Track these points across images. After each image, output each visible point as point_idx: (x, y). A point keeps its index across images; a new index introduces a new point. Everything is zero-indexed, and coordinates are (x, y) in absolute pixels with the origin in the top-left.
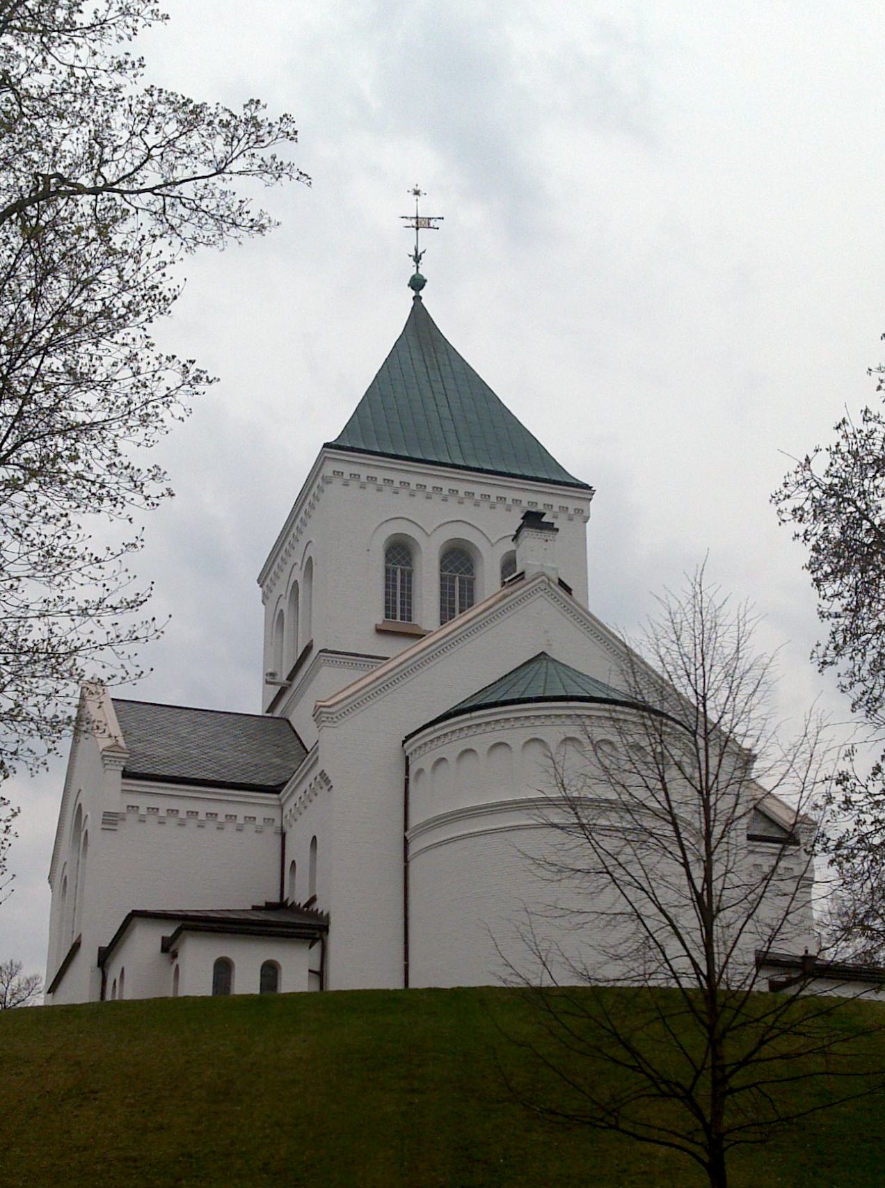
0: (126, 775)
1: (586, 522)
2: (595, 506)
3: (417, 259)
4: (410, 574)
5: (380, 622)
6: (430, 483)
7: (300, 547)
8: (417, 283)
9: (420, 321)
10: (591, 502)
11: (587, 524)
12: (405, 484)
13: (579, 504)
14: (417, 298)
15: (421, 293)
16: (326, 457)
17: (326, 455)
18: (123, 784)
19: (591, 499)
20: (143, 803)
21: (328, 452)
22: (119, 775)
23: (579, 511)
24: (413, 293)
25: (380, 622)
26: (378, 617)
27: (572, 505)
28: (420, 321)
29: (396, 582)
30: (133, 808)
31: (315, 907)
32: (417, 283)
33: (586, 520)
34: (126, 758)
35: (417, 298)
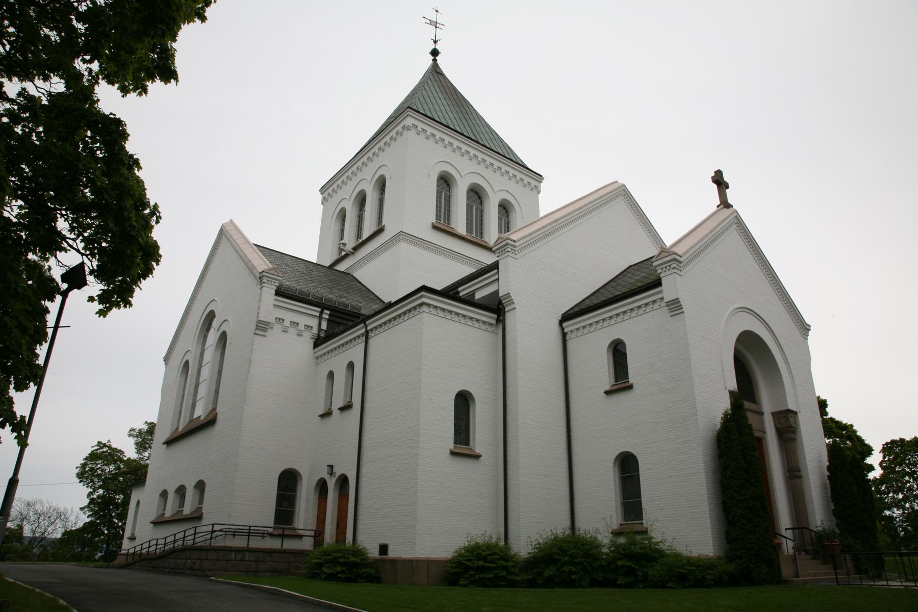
0: (279, 293)
1: (539, 194)
2: (543, 186)
3: (435, 42)
4: (450, 196)
5: (452, 447)
6: (430, 130)
7: (377, 162)
8: (435, 53)
9: (435, 71)
10: (541, 184)
11: (539, 195)
12: (424, 131)
13: (536, 183)
14: (435, 60)
15: (437, 58)
16: (408, 115)
17: (409, 113)
18: (275, 300)
19: (541, 182)
20: (289, 317)
21: (410, 112)
22: (274, 292)
23: (536, 187)
24: (433, 58)
25: (452, 447)
26: (451, 445)
27: (533, 183)
28: (435, 71)
29: (444, 217)
30: (280, 320)
31: (392, 554)
32: (435, 53)
33: (539, 192)
34: (280, 280)
35: (435, 60)
